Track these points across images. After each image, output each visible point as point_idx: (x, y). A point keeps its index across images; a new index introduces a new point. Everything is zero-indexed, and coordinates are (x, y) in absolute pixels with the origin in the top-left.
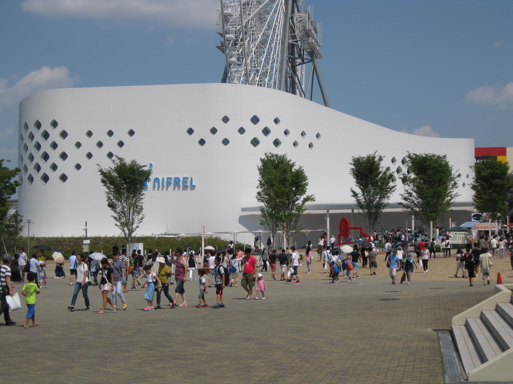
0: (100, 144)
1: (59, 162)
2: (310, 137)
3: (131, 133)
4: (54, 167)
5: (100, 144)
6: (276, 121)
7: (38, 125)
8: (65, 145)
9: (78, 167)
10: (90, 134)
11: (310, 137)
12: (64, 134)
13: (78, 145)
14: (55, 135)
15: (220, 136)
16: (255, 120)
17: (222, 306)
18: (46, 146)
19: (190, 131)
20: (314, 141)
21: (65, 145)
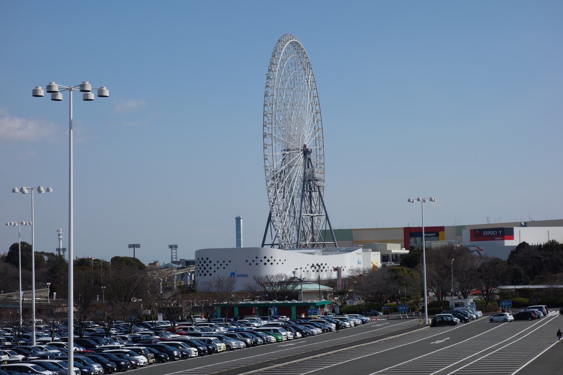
0: (221, 265)
1: (209, 270)
2: (283, 261)
3: (230, 261)
4: (208, 265)
5: (221, 265)
6: (250, 264)
7: (202, 259)
8: (211, 265)
9: (215, 271)
10: (218, 262)
11: (283, 261)
12: (210, 262)
13: (215, 265)
14: (207, 262)
15: (255, 262)
16: (211, 275)
17: (171, 247)
18: (205, 265)
19: (247, 261)
20: (284, 262)
21: (211, 265)
